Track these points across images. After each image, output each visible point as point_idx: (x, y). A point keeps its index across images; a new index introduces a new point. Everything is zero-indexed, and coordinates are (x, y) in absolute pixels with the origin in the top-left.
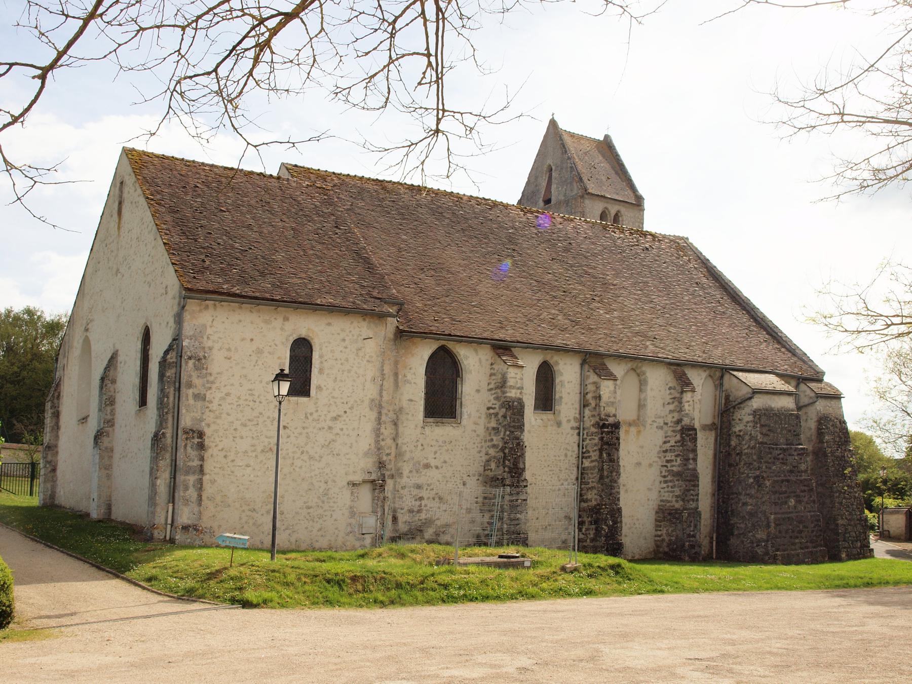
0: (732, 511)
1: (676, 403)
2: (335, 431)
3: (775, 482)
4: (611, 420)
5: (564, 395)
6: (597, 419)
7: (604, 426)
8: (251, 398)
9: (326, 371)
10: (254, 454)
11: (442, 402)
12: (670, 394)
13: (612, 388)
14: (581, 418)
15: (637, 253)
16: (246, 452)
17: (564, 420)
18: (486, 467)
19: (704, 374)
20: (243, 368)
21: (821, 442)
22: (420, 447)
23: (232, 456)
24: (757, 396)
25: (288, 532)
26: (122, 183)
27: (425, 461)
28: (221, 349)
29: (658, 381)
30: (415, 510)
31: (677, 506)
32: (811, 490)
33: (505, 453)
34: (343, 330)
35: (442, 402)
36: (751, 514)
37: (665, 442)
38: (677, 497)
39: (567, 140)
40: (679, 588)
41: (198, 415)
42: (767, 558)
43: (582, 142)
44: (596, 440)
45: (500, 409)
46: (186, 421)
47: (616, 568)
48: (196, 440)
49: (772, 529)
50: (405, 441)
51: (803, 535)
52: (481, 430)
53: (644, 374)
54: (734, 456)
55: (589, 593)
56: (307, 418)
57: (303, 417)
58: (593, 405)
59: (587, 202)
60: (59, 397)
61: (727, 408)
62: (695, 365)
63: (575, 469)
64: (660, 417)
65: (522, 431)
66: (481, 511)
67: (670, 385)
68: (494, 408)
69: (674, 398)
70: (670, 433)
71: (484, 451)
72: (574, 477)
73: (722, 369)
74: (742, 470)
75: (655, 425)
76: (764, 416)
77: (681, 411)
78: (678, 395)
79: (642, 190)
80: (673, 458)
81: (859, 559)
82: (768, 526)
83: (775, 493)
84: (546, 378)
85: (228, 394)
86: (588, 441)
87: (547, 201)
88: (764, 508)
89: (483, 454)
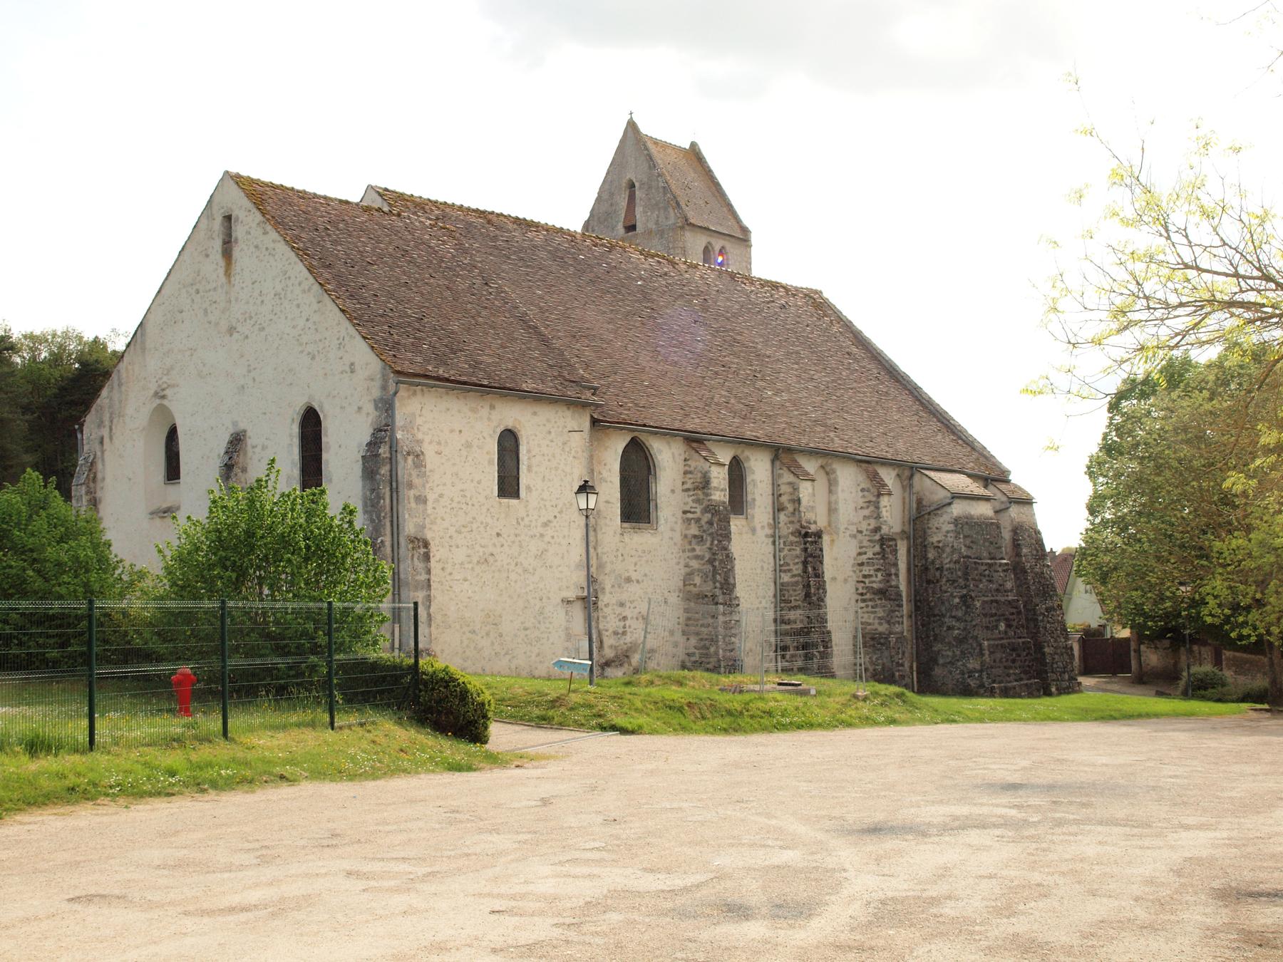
1: (872, 508)
2: (547, 539)
3: (984, 602)
4: (813, 528)
5: (757, 497)
6: (798, 526)
7: (806, 535)
9: (534, 469)
11: (636, 507)
16: (462, 563)
17: (758, 527)
21: (1018, 555)
24: (956, 501)
25: (508, 657)
26: (228, 218)
28: (430, 443)
31: (881, 629)
32: (1019, 613)
34: (548, 421)
35: (636, 507)
37: (860, 554)
38: (880, 618)
39: (653, 149)
42: (982, 691)
44: (798, 551)
46: (409, 527)
47: (899, 696)
48: (422, 550)
49: (987, 658)
51: (1018, 664)
53: (834, 472)
55: (892, 722)
59: (688, 234)
62: (885, 462)
63: (772, 585)
65: (729, 540)
66: (684, 633)
67: (863, 486)
70: (865, 543)
71: (682, 563)
72: (771, 593)
77: (878, 517)
79: (746, 221)
81: (1069, 693)
83: (985, 615)
84: (737, 472)
85: (441, 496)
87: (631, 228)
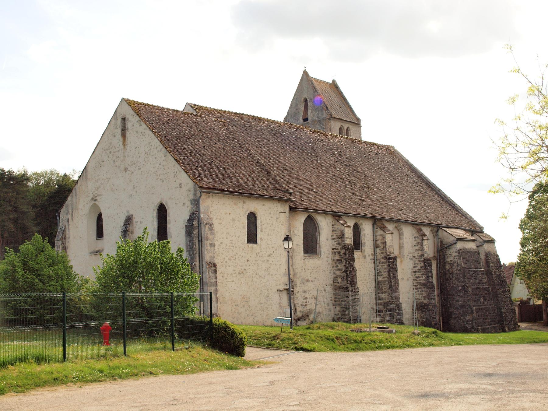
0: (450, 305)
2: (270, 262)
3: (473, 289)
4: (392, 255)
7: (389, 259)
9: (264, 230)
12: (415, 240)
13: (391, 238)
14: (375, 254)
15: (373, 157)
16: (231, 274)
18: (335, 280)
21: (488, 266)
22: (304, 270)
24: (459, 242)
25: (253, 317)
27: (307, 278)
28: (217, 219)
31: (425, 302)
32: (490, 293)
34: (270, 208)
36: (462, 306)
37: (414, 267)
39: (316, 84)
40: (467, 343)
41: (212, 255)
43: (323, 84)
44: (386, 266)
45: (341, 249)
46: (207, 258)
48: (213, 268)
52: (330, 261)
53: (402, 229)
54: (448, 274)
55: (432, 345)
59: (332, 122)
61: (442, 249)
62: (425, 224)
63: (374, 282)
64: (411, 253)
65: (354, 261)
66: (333, 305)
67: (415, 235)
68: (337, 249)
70: (417, 262)
71: (332, 273)
72: (374, 286)
73: (438, 227)
75: (409, 257)
77: (423, 250)
78: (420, 242)
79: (359, 115)
80: (420, 276)
82: (472, 313)
83: (474, 295)
85: (221, 243)
86: (380, 266)
87: (306, 120)
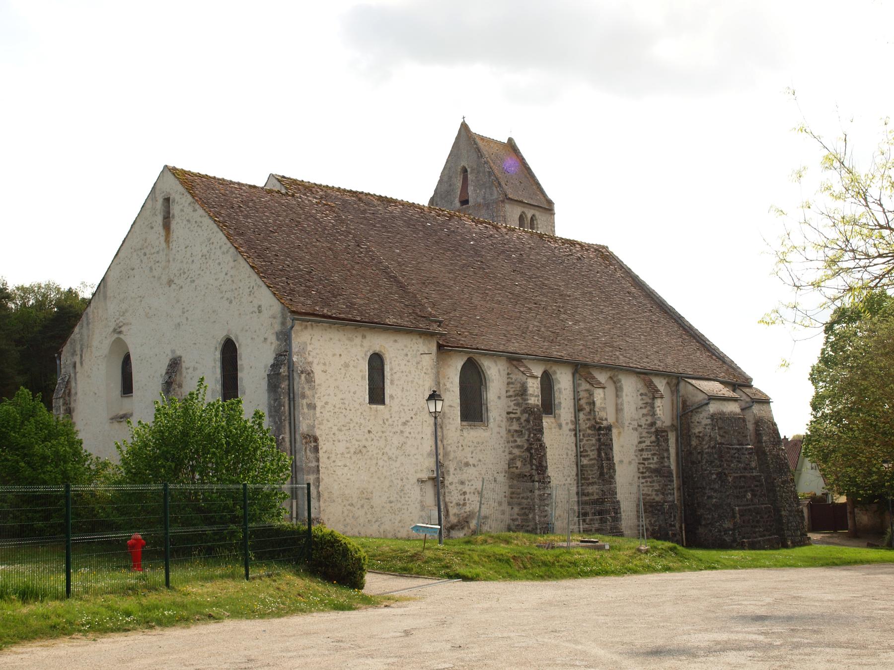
2: (406, 434)
3: (735, 478)
5: (563, 401)
6: (593, 422)
7: (600, 429)
8: (343, 406)
9: (396, 382)
10: (349, 455)
11: (473, 410)
12: (642, 399)
14: (576, 421)
15: (574, 263)
16: (342, 454)
17: (564, 423)
18: (511, 463)
19: (664, 382)
20: (336, 380)
22: (461, 448)
23: (333, 457)
24: (712, 402)
25: (378, 523)
27: (466, 460)
29: (630, 386)
30: (461, 503)
31: (657, 499)
33: (531, 454)
34: (406, 346)
41: (311, 422)
42: (735, 545)
44: (594, 441)
46: (303, 427)
48: (313, 444)
49: (738, 520)
50: (449, 442)
55: (668, 569)
56: (384, 423)
57: (381, 423)
58: (588, 410)
60: (69, 394)
65: (542, 433)
66: (509, 504)
67: (642, 391)
69: (647, 403)
70: (644, 434)
74: (704, 467)
75: (631, 426)
76: (718, 419)
77: (654, 414)
78: (650, 401)
79: (550, 195)
80: (650, 456)
82: (734, 517)
83: (736, 488)
84: (547, 383)
85: (326, 403)
86: (584, 442)
87: (464, 202)
88: (729, 501)
89: (506, 453)
